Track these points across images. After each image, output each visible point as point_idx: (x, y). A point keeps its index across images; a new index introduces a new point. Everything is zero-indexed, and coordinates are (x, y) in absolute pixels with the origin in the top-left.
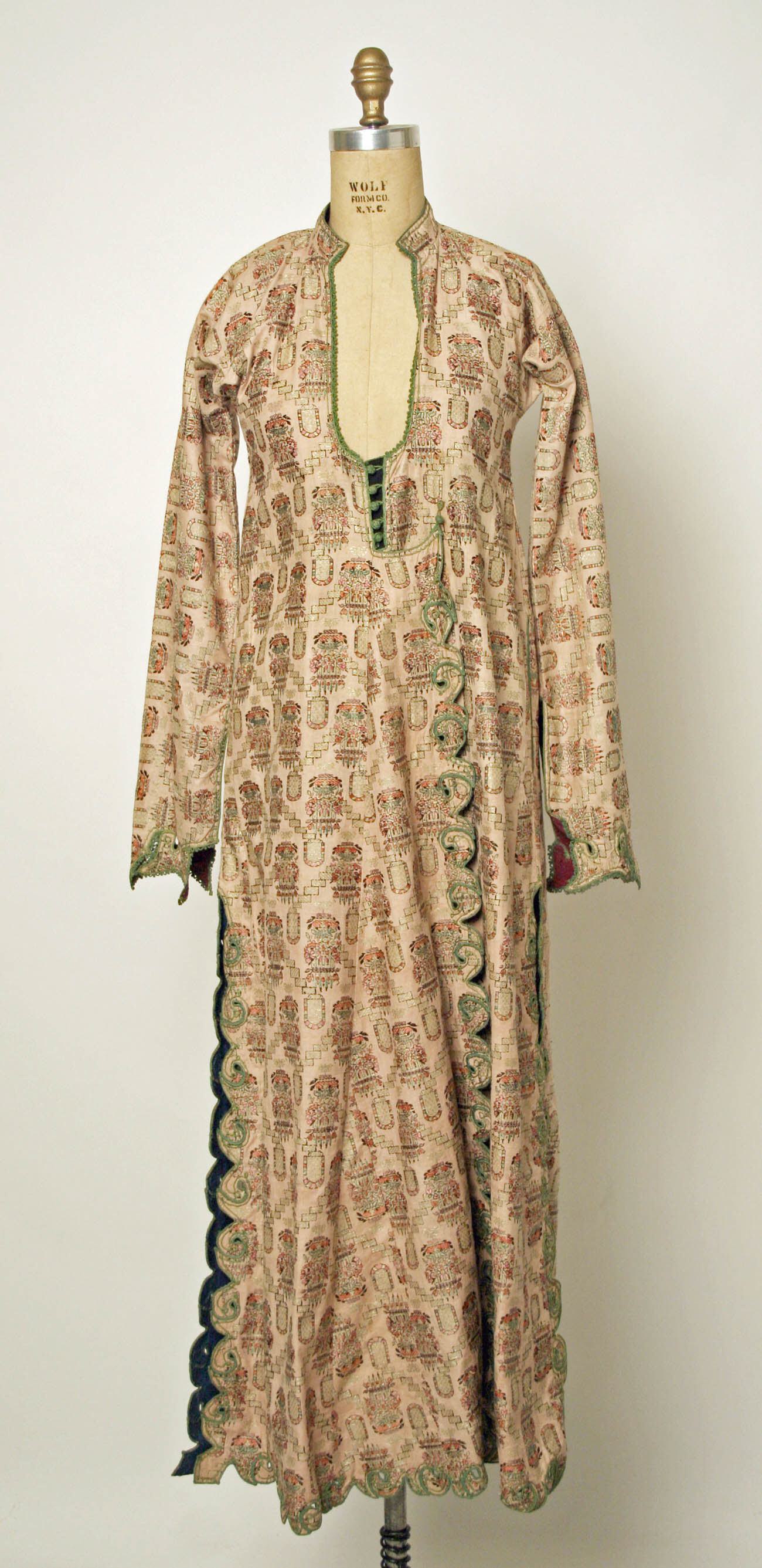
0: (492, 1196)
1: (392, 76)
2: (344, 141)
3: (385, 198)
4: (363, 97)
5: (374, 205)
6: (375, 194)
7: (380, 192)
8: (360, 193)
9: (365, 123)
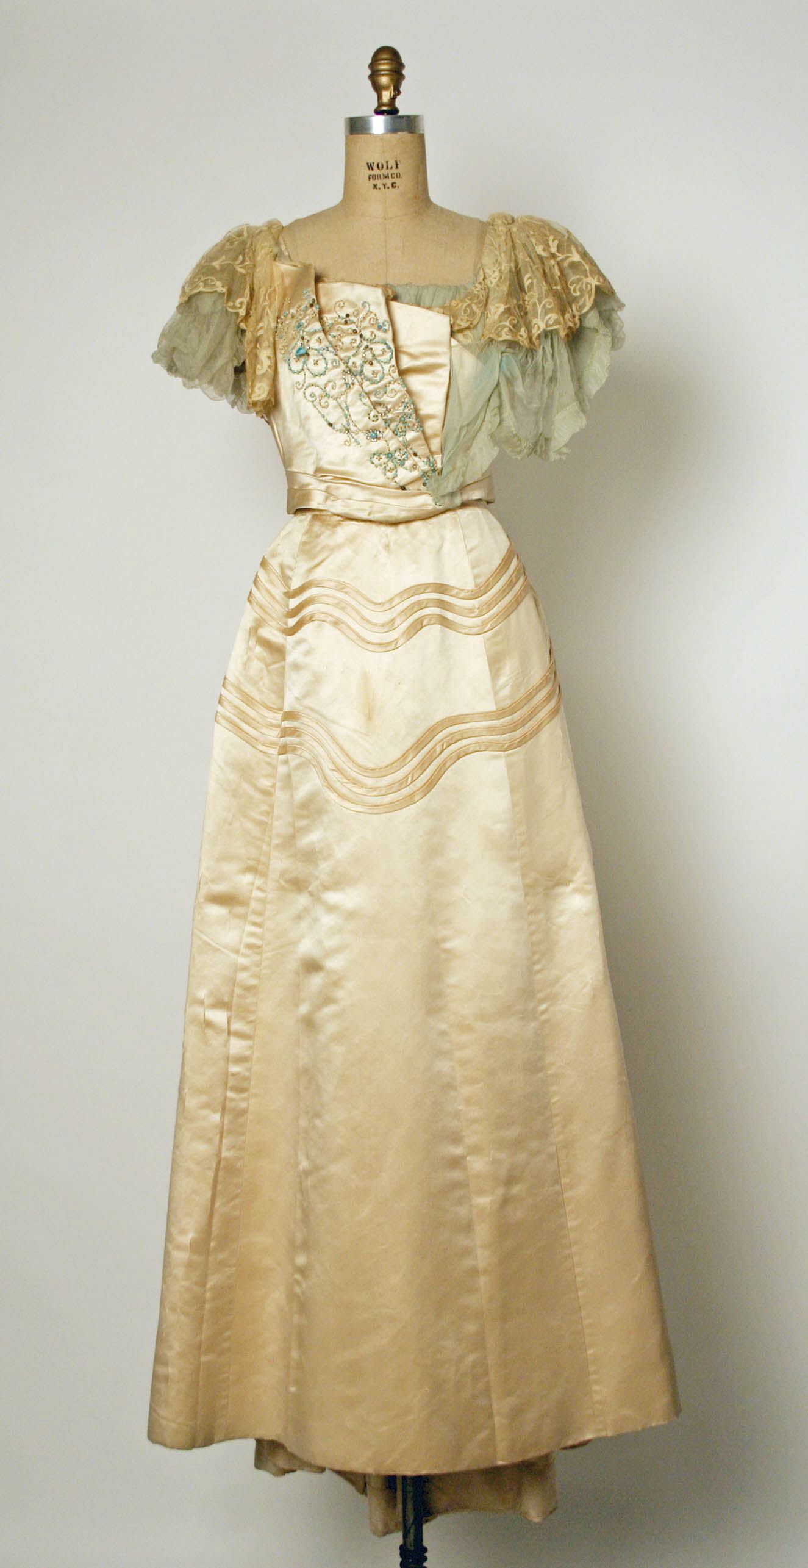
0: (332, 628)
1: (404, 72)
2: (356, 126)
3: (398, 176)
4: (378, 88)
5: (389, 182)
6: (390, 172)
7: (394, 171)
8: (376, 172)
9: (378, 112)
